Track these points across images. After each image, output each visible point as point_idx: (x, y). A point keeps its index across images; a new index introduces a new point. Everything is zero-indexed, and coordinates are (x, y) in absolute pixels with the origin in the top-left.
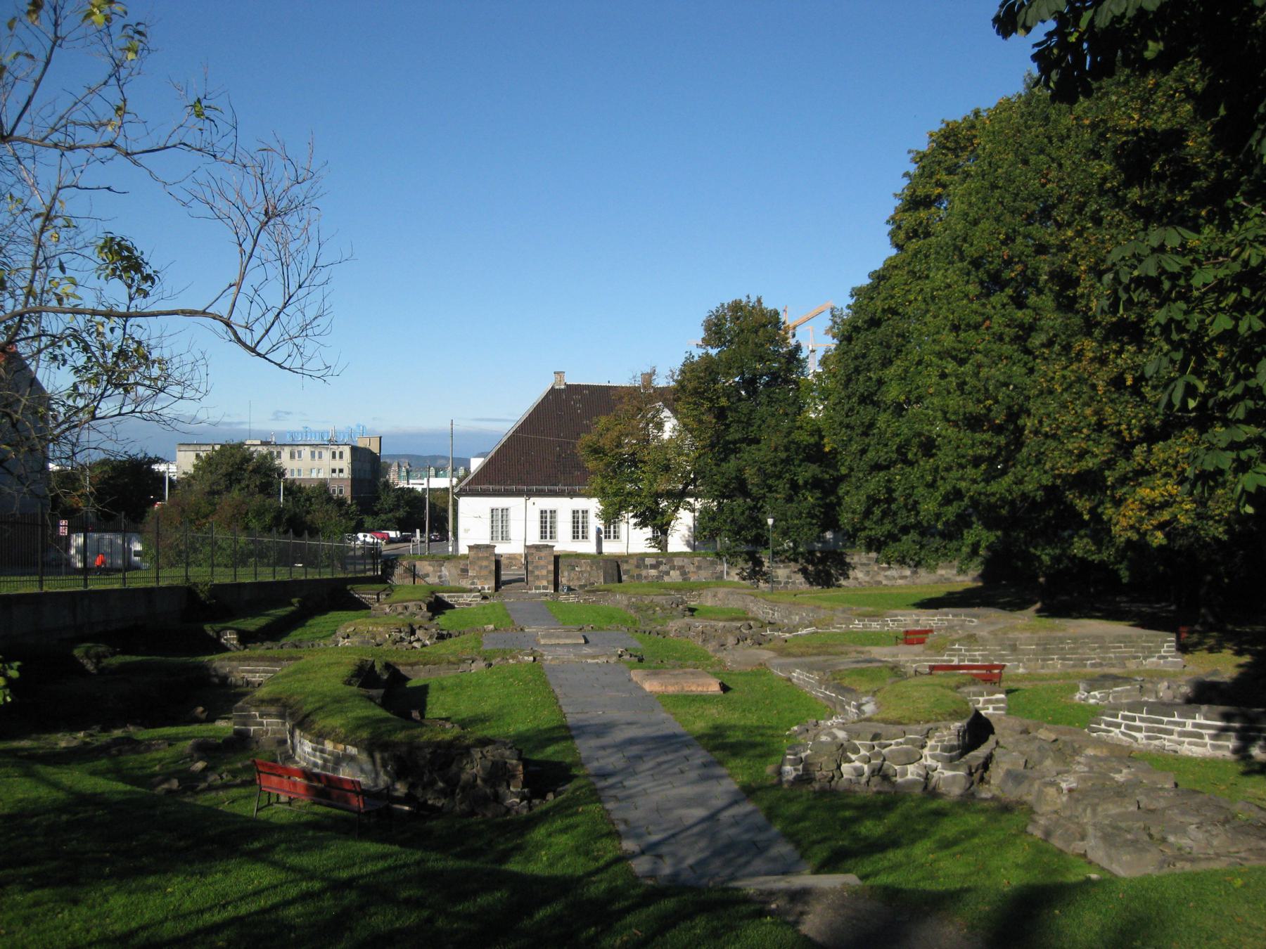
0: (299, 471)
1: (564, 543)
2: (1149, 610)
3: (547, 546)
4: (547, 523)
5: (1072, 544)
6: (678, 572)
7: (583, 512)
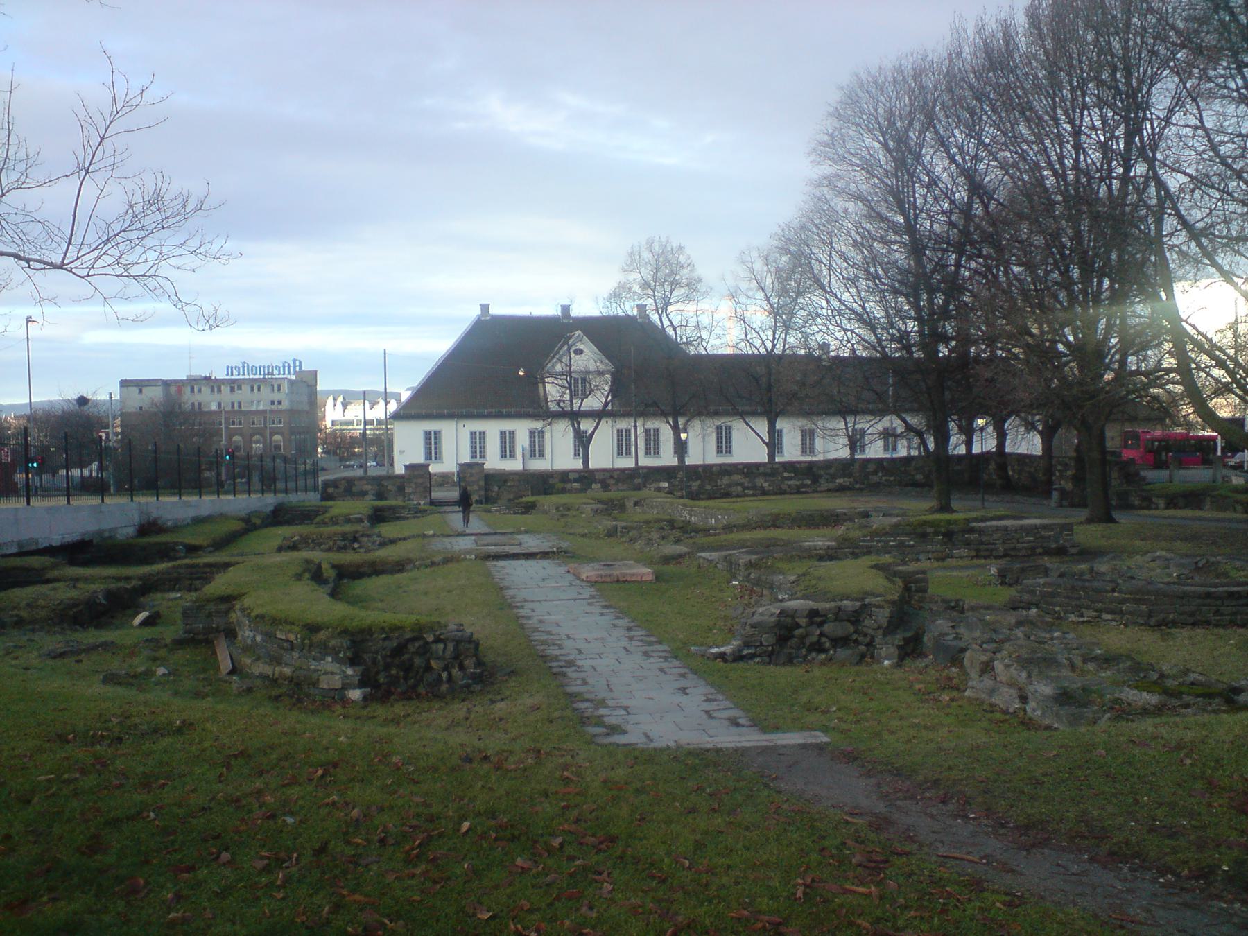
0: (240, 403)
1: (493, 462)
2: (838, 481)
3: (477, 464)
4: (478, 442)
5: (324, 660)
7: (435, 433)
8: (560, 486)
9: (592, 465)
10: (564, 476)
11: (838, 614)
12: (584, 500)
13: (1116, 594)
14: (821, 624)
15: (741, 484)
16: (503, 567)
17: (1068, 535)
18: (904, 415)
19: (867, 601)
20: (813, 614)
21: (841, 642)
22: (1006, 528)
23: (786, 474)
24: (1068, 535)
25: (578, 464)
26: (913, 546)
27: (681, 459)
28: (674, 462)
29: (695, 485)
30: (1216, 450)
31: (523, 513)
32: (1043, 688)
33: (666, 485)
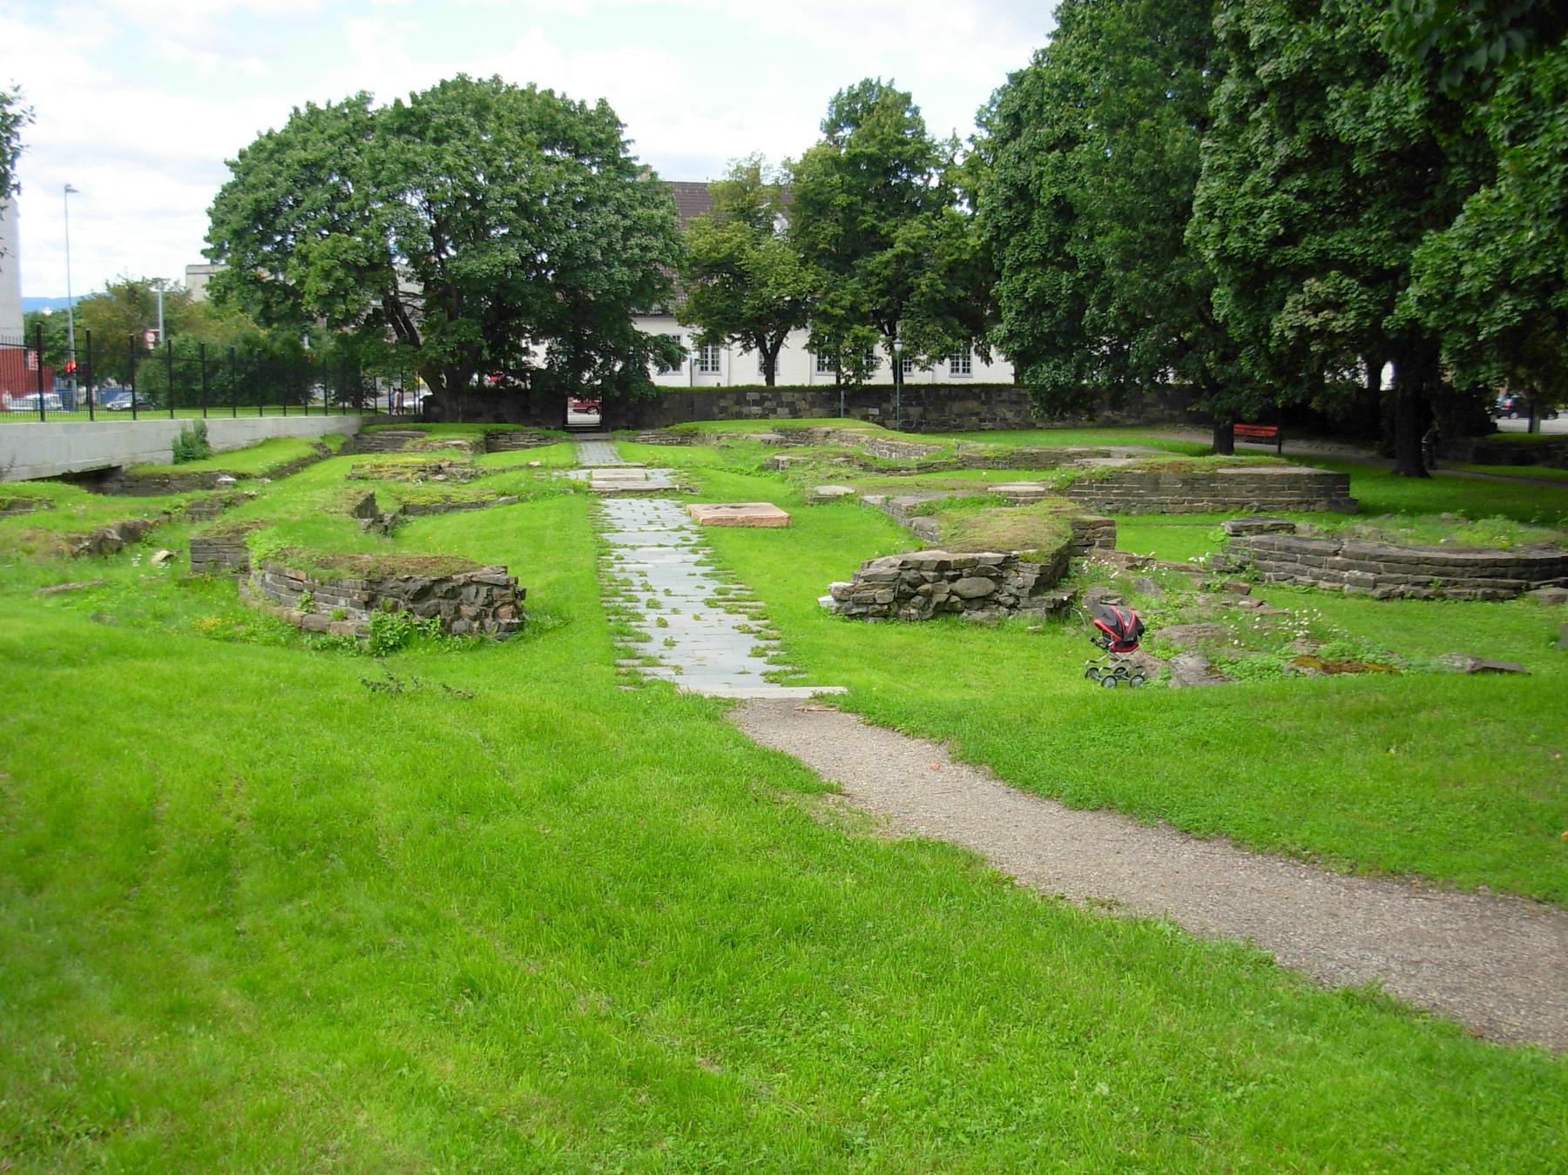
6: (787, 410)
8: (736, 409)
9: (779, 381)
11: (975, 569)
13: (1338, 558)
14: (953, 579)
15: (977, 414)
16: (606, 507)
20: (942, 566)
21: (985, 601)
22: (1262, 477)
25: (761, 381)
26: (1142, 496)
27: (770, 378)
28: (890, 381)
29: (914, 411)
31: (679, 444)
32: (1188, 660)
33: (876, 411)
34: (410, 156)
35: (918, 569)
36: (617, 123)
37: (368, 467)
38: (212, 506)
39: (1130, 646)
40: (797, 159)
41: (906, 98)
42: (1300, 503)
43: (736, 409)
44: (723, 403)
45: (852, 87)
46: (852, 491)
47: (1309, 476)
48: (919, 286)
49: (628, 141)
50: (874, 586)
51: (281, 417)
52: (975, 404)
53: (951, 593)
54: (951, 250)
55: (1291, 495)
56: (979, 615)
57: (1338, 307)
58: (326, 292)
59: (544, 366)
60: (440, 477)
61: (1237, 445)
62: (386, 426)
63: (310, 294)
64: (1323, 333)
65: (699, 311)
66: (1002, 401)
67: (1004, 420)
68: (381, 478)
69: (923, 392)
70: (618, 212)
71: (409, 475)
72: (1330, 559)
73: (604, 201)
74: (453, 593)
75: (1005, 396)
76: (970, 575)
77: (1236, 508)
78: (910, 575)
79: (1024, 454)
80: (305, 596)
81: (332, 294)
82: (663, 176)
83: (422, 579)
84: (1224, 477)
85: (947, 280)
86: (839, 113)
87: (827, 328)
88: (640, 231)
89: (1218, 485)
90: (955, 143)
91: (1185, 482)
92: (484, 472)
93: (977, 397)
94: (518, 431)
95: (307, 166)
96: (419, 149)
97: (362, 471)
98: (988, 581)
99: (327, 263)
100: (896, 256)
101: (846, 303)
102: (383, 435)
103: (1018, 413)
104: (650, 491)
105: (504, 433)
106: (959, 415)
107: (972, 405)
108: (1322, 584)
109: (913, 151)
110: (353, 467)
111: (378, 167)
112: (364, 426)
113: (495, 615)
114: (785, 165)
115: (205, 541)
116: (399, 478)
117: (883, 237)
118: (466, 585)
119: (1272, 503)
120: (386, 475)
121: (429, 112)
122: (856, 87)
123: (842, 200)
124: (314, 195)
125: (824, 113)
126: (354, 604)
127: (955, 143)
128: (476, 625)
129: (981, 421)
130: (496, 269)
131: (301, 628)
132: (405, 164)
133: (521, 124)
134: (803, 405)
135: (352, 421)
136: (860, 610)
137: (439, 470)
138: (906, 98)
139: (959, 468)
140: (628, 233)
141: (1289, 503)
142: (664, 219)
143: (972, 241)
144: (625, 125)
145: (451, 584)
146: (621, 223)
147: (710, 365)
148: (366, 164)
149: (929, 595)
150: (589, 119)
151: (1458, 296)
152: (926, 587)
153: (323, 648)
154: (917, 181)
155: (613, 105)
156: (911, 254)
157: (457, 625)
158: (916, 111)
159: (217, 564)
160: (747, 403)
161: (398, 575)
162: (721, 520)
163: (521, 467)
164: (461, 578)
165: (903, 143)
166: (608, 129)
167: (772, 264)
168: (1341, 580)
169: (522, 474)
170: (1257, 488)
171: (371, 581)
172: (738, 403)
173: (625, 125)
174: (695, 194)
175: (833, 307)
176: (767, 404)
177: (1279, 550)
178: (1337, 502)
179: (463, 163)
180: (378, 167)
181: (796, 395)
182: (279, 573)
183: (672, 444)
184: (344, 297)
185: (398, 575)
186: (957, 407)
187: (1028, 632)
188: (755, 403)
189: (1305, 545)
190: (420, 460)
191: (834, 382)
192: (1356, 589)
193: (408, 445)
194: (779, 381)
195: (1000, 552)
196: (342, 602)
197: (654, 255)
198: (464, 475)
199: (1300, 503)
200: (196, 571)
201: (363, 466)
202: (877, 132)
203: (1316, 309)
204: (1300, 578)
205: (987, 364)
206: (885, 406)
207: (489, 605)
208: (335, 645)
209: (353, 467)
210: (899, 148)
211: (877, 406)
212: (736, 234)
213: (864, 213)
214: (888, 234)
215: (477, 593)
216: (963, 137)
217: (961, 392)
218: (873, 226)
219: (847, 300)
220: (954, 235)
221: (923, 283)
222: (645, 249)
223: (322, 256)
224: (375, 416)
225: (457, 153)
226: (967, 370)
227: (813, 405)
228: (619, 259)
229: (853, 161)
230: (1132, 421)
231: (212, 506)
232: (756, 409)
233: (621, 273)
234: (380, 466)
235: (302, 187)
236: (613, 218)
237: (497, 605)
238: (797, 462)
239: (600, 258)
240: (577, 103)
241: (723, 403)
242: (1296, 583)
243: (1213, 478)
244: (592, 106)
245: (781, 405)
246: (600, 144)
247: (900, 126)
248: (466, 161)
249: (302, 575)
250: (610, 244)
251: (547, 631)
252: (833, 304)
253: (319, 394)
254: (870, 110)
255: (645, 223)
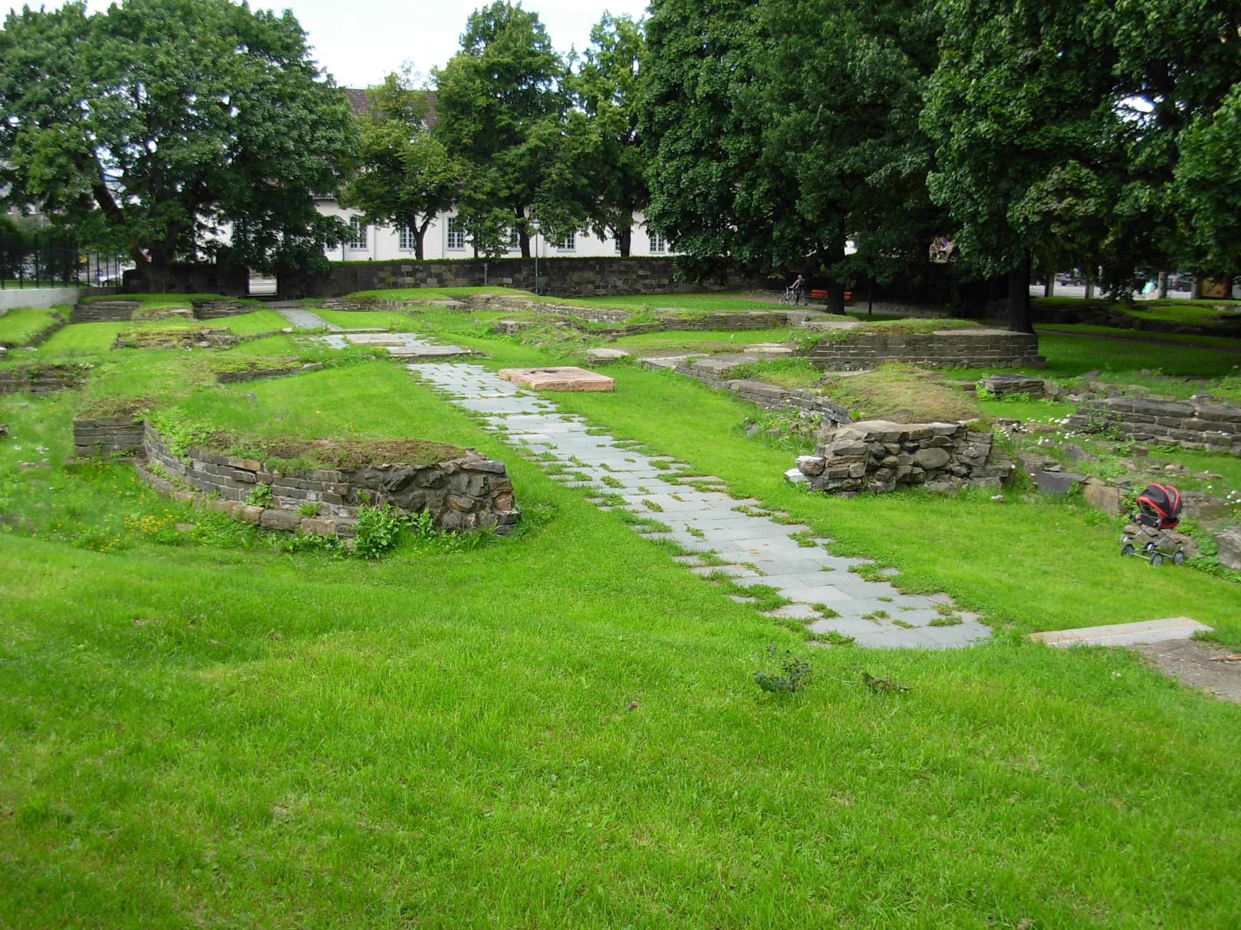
8: (393, 279)
9: (427, 256)
10: (395, 266)
11: (930, 439)
12: (438, 296)
13: (1194, 419)
14: (912, 451)
15: (593, 282)
17: (1031, 348)
18: (419, 230)
19: (962, 422)
20: (903, 438)
21: (939, 472)
22: (969, 338)
23: (641, 273)
24: (1031, 348)
25: (411, 255)
30: (686, 257)
31: (359, 310)
34: (125, 53)
35: (880, 441)
36: (300, 31)
37: (134, 335)
38: (20, 377)
39: (1170, 522)
40: (443, 67)
41: (534, 17)
42: (1000, 360)
43: (393, 279)
44: (381, 275)
45: (485, 7)
46: (627, 354)
47: (1006, 337)
48: (550, 175)
49: (310, 47)
50: (847, 460)
51: (19, 290)
52: (591, 274)
53: (916, 465)
54: (577, 145)
55: (992, 354)
56: (942, 486)
57: (1080, 194)
58: (50, 177)
59: (229, 244)
60: (204, 344)
61: (846, 309)
62: (102, 297)
63: (34, 178)
64: (1064, 218)
65: (362, 196)
66: (614, 272)
67: (615, 287)
68: (149, 345)
69: (548, 264)
70: (305, 107)
71: (175, 342)
72: (1186, 420)
73: (293, 98)
74: (440, 483)
75: (615, 267)
76: (928, 446)
77: (950, 365)
78: (876, 448)
79: (716, 317)
80: (260, 488)
81: (56, 179)
82: (342, 81)
83: (404, 468)
84: (940, 338)
85: (573, 170)
86: (475, 29)
87: (471, 211)
88: (324, 125)
89: (935, 346)
90: (573, 56)
91: (908, 343)
92: (242, 339)
93: (592, 268)
94: (220, 300)
95: (25, 62)
96: (132, 49)
97: (128, 340)
98: (944, 451)
99: (50, 151)
100: (530, 150)
101: (487, 188)
102: (98, 305)
103: (626, 282)
104: (447, 356)
105: (207, 302)
106: (578, 284)
107: (589, 275)
108: (1183, 443)
109: (542, 61)
110: (119, 335)
111: (96, 64)
112: (83, 297)
113: (494, 506)
114: (432, 72)
115: (91, 423)
116: (165, 345)
117: (517, 133)
118: (455, 473)
119: (979, 361)
120: (153, 342)
121: (140, 15)
122: (490, 7)
123: (482, 101)
124: (33, 89)
125: (462, 28)
126: (328, 498)
127: (573, 56)
128: (472, 518)
129: (596, 287)
130: (205, 157)
131: (260, 527)
132: (120, 61)
133: (220, 28)
134: (448, 276)
135: (72, 292)
136: (836, 485)
137: (201, 338)
138: (534, 17)
139: (661, 330)
140: (315, 125)
141: (992, 361)
142: (344, 114)
143: (594, 137)
144: (308, 33)
145: (438, 473)
146: (309, 117)
147: (657, 247)
148: (84, 62)
149: (894, 467)
150: (276, 27)
151: (1230, 182)
152: (891, 459)
153: (296, 549)
154: (541, 87)
155: (296, 15)
156: (543, 148)
157: (449, 518)
158: (541, 28)
159: (104, 449)
160: (402, 274)
161: (375, 463)
162: (553, 385)
163: (275, 334)
164: (450, 465)
165: (533, 54)
166: (294, 35)
167: (425, 156)
168: (1201, 440)
169: (280, 341)
170: (966, 348)
171: (343, 471)
172: (394, 274)
173: (308, 33)
174: (359, 97)
175: (475, 192)
176: (419, 275)
177: (1137, 411)
178: (1029, 360)
179: (174, 62)
180: (96, 64)
181: (443, 267)
182: (220, 463)
183: (353, 310)
184: (66, 182)
185: (375, 463)
186: (576, 277)
187: (994, 501)
188: (409, 274)
189: (1161, 407)
190: (184, 328)
191: (472, 256)
192: (1216, 449)
193: (136, 314)
194: (427, 256)
195: (947, 422)
196: (312, 496)
197: (338, 146)
198: (225, 341)
199: (1000, 360)
200: (82, 455)
201: (129, 335)
202: (512, 45)
203: (1060, 194)
204: (1160, 438)
205: (603, 241)
206: (517, 276)
207: (486, 495)
208: (311, 546)
209: (119, 335)
210: (531, 59)
211: (510, 276)
212: (393, 129)
213: (501, 113)
214: (522, 131)
215: (470, 482)
216: (580, 50)
217: (580, 265)
218: (509, 125)
219: (488, 187)
220: (577, 132)
221: (554, 171)
222: (330, 140)
223: (45, 145)
224: (87, 291)
225: (168, 53)
226: (571, 246)
227: (457, 275)
228: (307, 149)
229: (491, 69)
230: (717, 288)
231: (20, 377)
232: (409, 280)
233: (311, 161)
234: (146, 334)
235: (23, 82)
236: (304, 113)
237: (496, 493)
238: (524, 325)
239: (292, 148)
240: (265, 13)
241: (381, 275)
242: (1157, 442)
243: (931, 339)
244: (278, 15)
245: (430, 275)
246: (288, 48)
247: (530, 40)
248: (177, 61)
249: (255, 465)
250: (300, 136)
251: (547, 521)
252: (475, 189)
253: (30, 270)
254: (501, 26)
255: (328, 118)
